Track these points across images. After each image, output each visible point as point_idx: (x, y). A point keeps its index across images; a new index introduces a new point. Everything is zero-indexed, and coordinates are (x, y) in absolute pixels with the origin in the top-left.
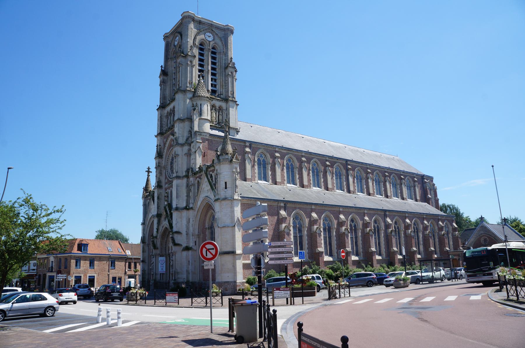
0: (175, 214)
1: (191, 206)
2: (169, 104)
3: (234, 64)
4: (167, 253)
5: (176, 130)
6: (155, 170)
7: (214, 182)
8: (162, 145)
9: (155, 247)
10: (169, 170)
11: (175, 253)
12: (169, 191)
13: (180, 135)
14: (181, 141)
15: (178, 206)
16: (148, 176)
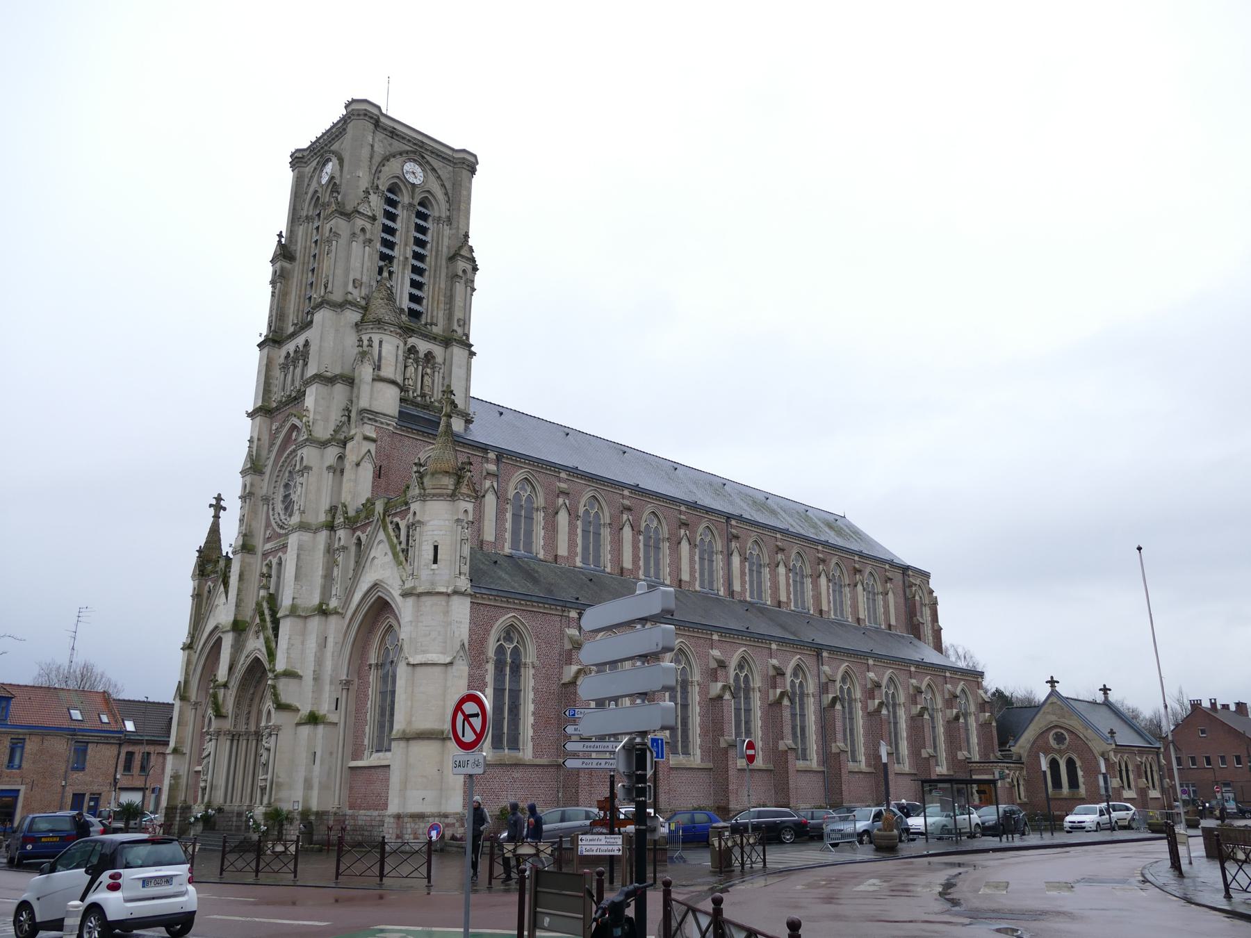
0: (285, 627)
1: (333, 603)
2: (293, 335)
3: (471, 250)
4: (253, 728)
5: (309, 401)
6: (239, 503)
7: (404, 546)
8: (265, 438)
9: (219, 715)
10: (279, 507)
11: (278, 728)
12: (275, 561)
13: (318, 417)
14: (323, 431)
15: (298, 602)
16: (217, 517)
